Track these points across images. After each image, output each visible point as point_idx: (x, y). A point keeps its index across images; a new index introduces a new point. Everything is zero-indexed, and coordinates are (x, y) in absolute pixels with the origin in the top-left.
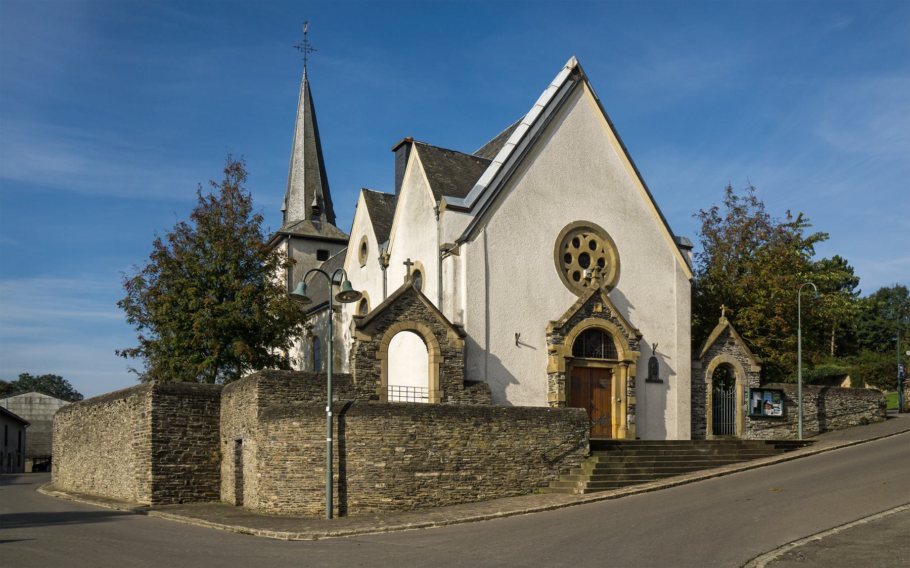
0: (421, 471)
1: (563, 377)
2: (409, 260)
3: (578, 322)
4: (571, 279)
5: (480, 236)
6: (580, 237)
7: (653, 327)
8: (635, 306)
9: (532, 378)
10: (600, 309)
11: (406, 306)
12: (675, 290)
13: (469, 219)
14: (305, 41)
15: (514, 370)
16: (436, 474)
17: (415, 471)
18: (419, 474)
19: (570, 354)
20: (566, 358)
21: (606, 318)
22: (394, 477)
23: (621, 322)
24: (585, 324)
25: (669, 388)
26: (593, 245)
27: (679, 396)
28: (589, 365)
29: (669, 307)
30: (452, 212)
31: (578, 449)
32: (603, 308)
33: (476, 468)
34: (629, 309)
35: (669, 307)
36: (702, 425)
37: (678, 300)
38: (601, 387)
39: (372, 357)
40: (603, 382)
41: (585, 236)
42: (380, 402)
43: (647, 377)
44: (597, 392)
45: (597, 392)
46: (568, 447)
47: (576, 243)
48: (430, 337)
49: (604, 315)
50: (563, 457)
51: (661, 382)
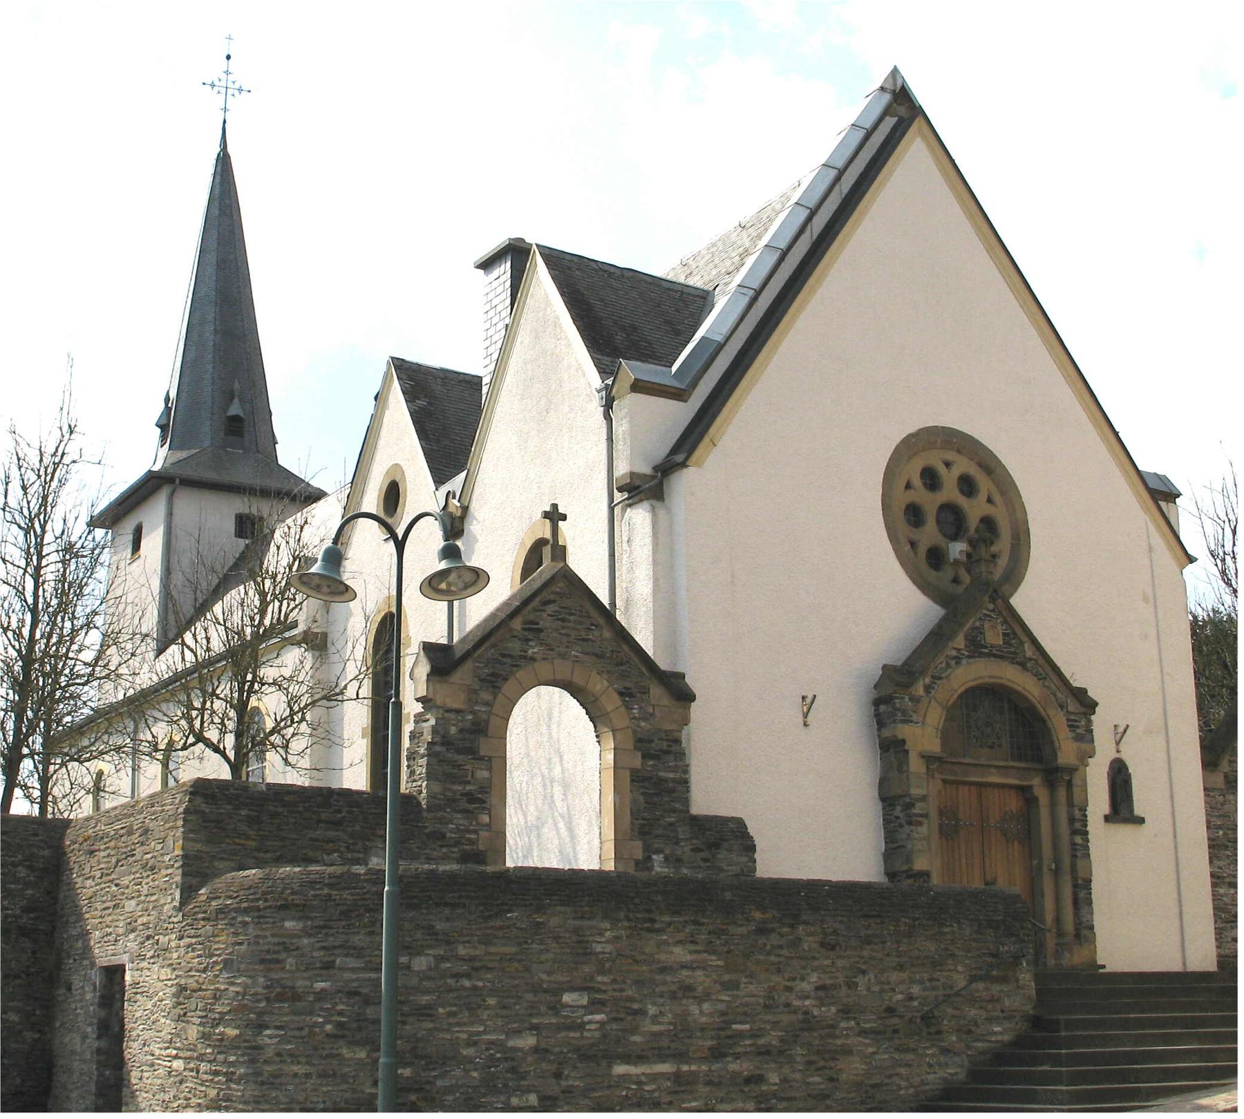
0: (627, 1059)
2: (555, 506)
4: (926, 565)
9: (809, 809)
11: (556, 626)
13: (679, 414)
14: (227, 73)
16: (666, 1068)
17: (612, 1058)
18: (620, 1069)
22: (558, 1075)
33: (765, 1052)
39: (472, 752)
42: (489, 869)
48: (612, 702)
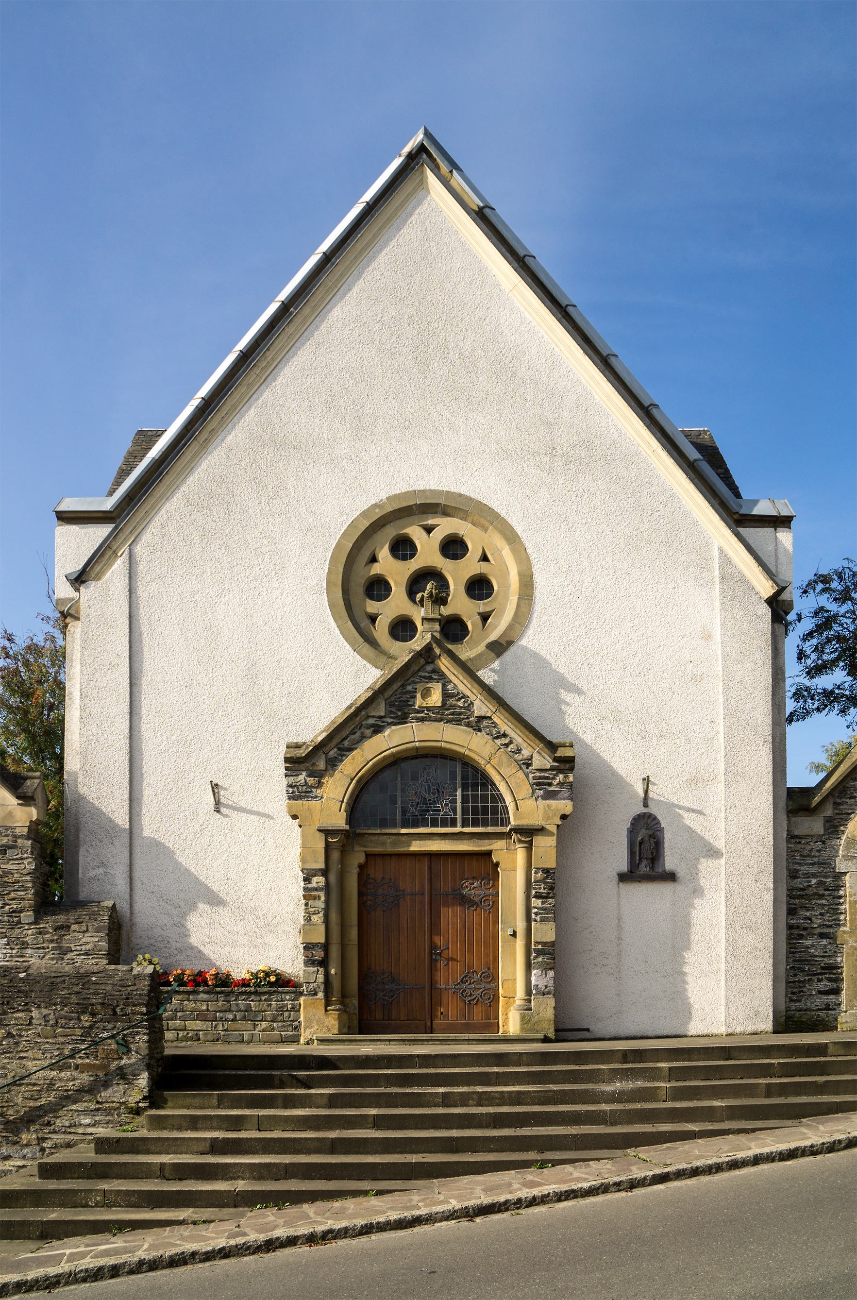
1: (318, 881)
3: (363, 738)
5: (119, 566)
6: (415, 533)
7: (644, 735)
8: (583, 684)
10: (435, 698)
12: (718, 638)
15: (212, 876)
19: (339, 821)
20: (327, 833)
21: (458, 722)
23: (503, 724)
24: (393, 739)
25: (698, 891)
26: (453, 547)
27: (733, 913)
28: (416, 846)
29: (697, 679)
30: (74, 529)
31: (106, 1085)
32: (446, 695)
34: (564, 695)
35: (697, 679)
36: (824, 985)
37: (726, 657)
38: (465, 901)
40: (472, 889)
41: (429, 530)
43: (624, 867)
44: (451, 916)
45: (451, 916)
46: (72, 1079)
47: (403, 548)
49: (453, 711)
50: (54, 1109)
51: (671, 877)
